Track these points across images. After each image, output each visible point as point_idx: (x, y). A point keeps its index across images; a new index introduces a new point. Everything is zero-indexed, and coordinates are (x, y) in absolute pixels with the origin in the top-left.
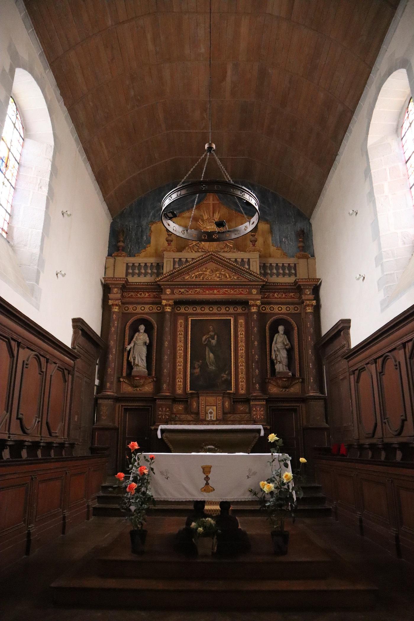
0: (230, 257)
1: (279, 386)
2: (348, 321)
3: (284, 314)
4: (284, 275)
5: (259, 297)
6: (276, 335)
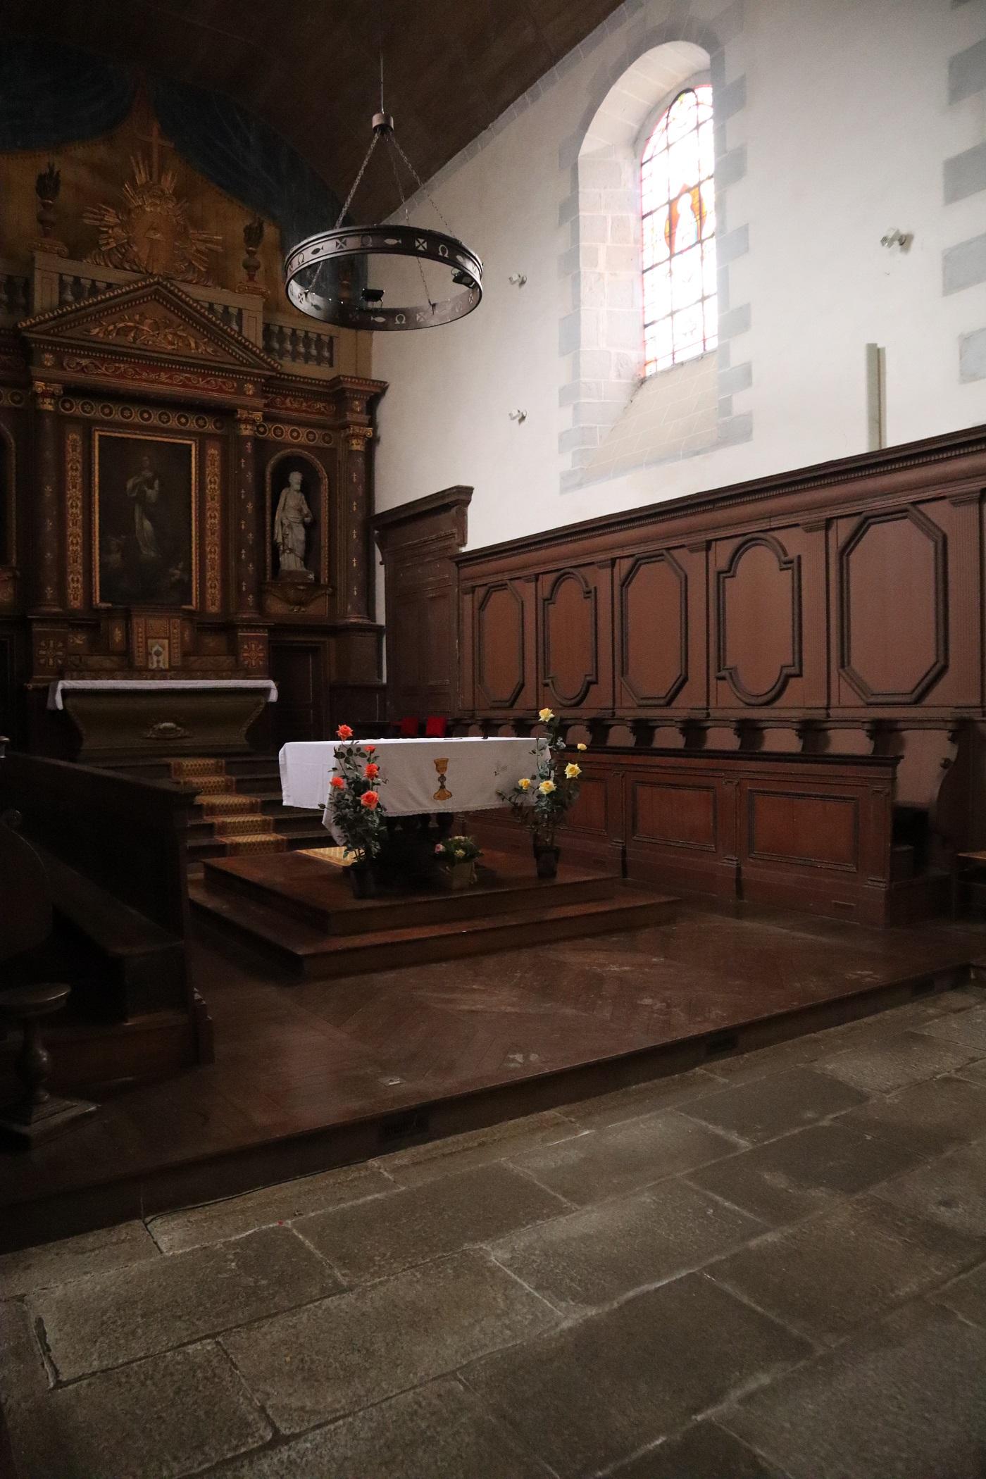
0: (199, 298)
1: (288, 601)
2: (468, 491)
3: (300, 446)
4: (308, 357)
5: (260, 402)
6: (284, 492)
